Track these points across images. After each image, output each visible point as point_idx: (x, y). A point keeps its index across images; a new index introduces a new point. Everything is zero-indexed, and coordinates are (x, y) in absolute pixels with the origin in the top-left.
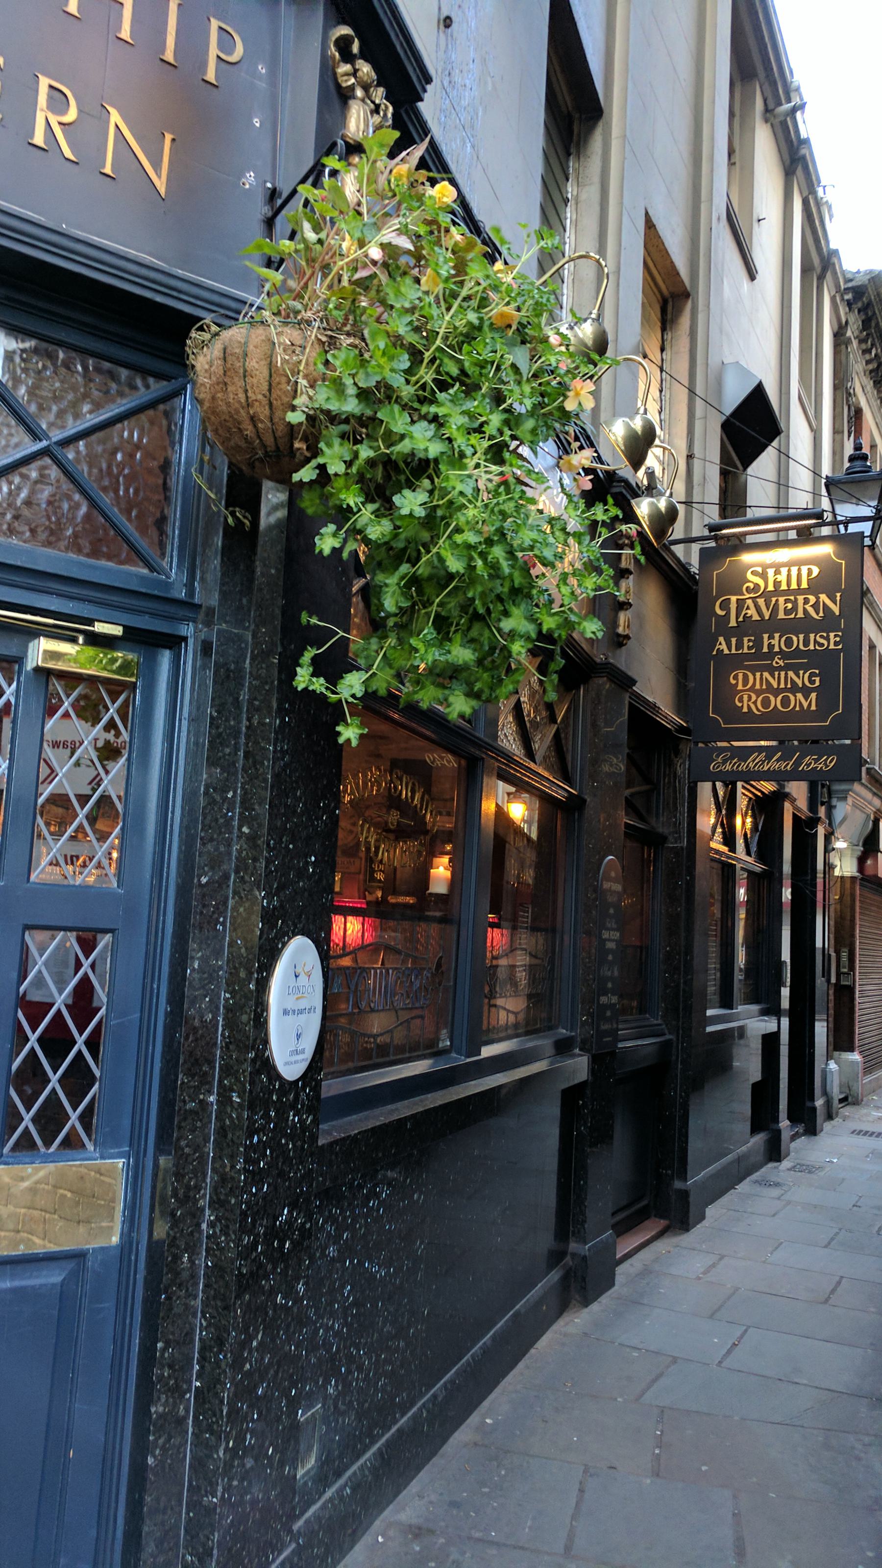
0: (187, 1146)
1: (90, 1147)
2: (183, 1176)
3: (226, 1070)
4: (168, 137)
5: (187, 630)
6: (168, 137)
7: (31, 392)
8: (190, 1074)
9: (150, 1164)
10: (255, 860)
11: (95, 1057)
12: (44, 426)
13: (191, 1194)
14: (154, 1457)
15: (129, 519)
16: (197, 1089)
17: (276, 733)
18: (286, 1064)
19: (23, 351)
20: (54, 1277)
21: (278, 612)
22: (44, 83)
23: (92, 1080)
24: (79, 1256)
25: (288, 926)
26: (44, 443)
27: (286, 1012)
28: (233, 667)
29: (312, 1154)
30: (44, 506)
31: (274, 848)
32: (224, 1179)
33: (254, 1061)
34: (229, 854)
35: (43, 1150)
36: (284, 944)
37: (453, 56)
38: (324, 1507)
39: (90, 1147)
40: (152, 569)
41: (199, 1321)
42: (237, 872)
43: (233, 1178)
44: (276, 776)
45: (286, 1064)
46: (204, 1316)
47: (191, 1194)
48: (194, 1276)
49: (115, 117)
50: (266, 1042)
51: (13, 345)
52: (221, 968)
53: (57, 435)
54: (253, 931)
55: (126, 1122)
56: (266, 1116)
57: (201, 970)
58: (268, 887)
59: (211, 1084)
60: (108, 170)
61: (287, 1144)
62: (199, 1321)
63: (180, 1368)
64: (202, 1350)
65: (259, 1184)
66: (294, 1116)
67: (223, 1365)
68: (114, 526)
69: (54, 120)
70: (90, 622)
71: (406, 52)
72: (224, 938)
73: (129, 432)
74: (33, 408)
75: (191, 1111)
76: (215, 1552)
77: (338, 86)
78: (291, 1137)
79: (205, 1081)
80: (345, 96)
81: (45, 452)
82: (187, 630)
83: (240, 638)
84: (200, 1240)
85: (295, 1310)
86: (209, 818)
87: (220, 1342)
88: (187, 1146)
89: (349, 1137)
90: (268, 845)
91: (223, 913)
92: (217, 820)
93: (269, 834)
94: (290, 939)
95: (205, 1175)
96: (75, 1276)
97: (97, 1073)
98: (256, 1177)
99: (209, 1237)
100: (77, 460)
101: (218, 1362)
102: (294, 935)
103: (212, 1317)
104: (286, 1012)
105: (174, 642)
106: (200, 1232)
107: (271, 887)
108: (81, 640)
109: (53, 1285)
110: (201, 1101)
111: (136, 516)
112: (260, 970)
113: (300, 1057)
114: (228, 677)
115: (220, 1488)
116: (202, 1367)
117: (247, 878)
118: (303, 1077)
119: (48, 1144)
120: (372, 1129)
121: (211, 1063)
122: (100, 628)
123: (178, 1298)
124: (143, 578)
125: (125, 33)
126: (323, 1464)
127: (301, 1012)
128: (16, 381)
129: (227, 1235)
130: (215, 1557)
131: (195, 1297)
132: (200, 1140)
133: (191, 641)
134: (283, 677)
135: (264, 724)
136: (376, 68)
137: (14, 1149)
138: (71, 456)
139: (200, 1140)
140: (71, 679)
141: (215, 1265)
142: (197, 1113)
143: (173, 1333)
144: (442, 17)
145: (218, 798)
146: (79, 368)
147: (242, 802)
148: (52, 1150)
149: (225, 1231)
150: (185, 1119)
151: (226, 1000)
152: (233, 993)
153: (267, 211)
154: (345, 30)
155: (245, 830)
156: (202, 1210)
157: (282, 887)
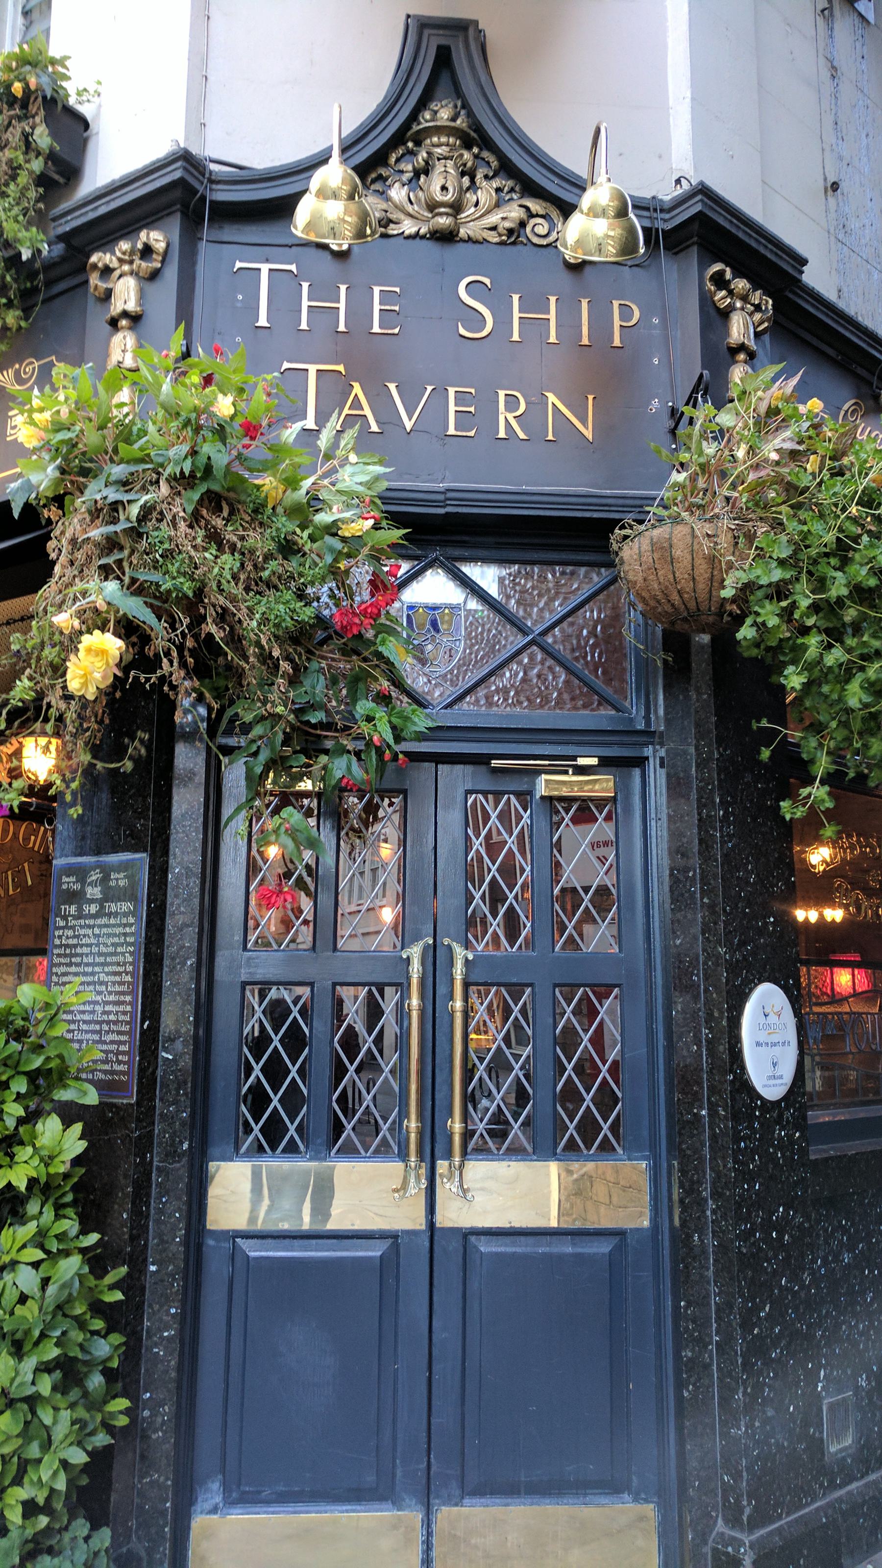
0: (688, 1148)
1: (620, 1151)
2: (687, 1172)
3: (712, 1090)
4: (590, 397)
5: (648, 751)
6: (590, 397)
7: (518, 602)
8: (683, 1092)
9: (665, 1165)
10: (715, 923)
11: (617, 1083)
12: (529, 624)
13: (695, 1187)
14: (688, 1390)
15: (597, 676)
16: (691, 1105)
17: (721, 821)
18: (765, 1086)
19: (510, 575)
20: (604, 1247)
21: (713, 727)
22: (502, 394)
23: (616, 1100)
24: (619, 1233)
25: (753, 975)
26: (531, 637)
27: (758, 1044)
28: (682, 775)
29: (803, 1165)
30: (535, 681)
31: (729, 914)
32: (718, 1176)
33: (732, 1082)
34: (695, 920)
35: (585, 1152)
36: (751, 990)
37: (847, 209)
38: (866, 1485)
39: (620, 1151)
40: (618, 710)
41: (713, 1289)
42: (703, 934)
43: (726, 1175)
44: (725, 856)
45: (765, 1086)
46: (716, 1285)
47: (695, 1187)
48: (704, 1252)
49: (552, 398)
50: (743, 1068)
51: (504, 572)
52: (699, 1010)
53: (539, 629)
54: (720, 980)
55: (645, 1133)
56: (751, 1127)
57: (684, 1011)
58: (729, 944)
59: (701, 1100)
60: (550, 437)
61: (775, 1153)
62: (713, 1289)
63: (702, 1324)
64: (718, 1311)
65: (751, 1182)
66: (780, 1130)
67: (734, 1324)
68: (586, 684)
69: (510, 417)
70: (574, 758)
71: (776, 254)
72: (699, 986)
73: (591, 613)
74: (521, 613)
75: (688, 1122)
76: (745, 1474)
77: (718, 309)
78: (780, 1147)
79: (696, 1098)
80: (725, 314)
81: (532, 642)
82: (648, 751)
83: (685, 752)
84: (706, 1223)
85: (803, 1295)
86: (676, 893)
87: (730, 1305)
88: (688, 1148)
89: (845, 1156)
90: (724, 910)
91: (696, 967)
92: (682, 895)
93: (724, 902)
94: (756, 985)
95: (705, 1173)
96: (620, 1249)
97: (620, 1095)
98: (751, 1177)
99: (713, 1222)
100: (555, 642)
101: (730, 1321)
102: (761, 981)
103: (722, 1286)
104: (758, 1044)
105: (640, 762)
106: (706, 1217)
107: (732, 944)
108: (570, 772)
109: (603, 1254)
110: (695, 1114)
111: (603, 673)
112: (729, 1009)
113: (779, 1081)
114: (679, 783)
115: (742, 1423)
116: (719, 1325)
117: (711, 938)
118: (785, 1098)
119: (589, 1148)
120: (872, 1152)
121: (700, 1084)
122: (582, 761)
123: (694, 1268)
124: (611, 718)
125: (553, 339)
126: (862, 1448)
127: (774, 1045)
128: (508, 597)
129: (726, 1221)
130: (745, 1478)
131: (708, 1269)
132: (698, 1145)
133: (651, 760)
134: (722, 777)
135: (711, 816)
136: (750, 280)
137: (564, 1150)
138: (550, 640)
139: (698, 1145)
140: (568, 801)
141: (720, 1245)
142: (693, 1123)
143: (693, 1295)
144: (829, 185)
145: (681, 877)
146: (550, 576)
147: (701, 879)
148: (592, 1152)
149: (724, 1217)
150: (684, 1128)
151: (707, 1035)
152: (710, 1029)
153: (671, 424)
154: (717, 267)
155: (706, 900)
156: (706, 1200)
157: (743, 943)
